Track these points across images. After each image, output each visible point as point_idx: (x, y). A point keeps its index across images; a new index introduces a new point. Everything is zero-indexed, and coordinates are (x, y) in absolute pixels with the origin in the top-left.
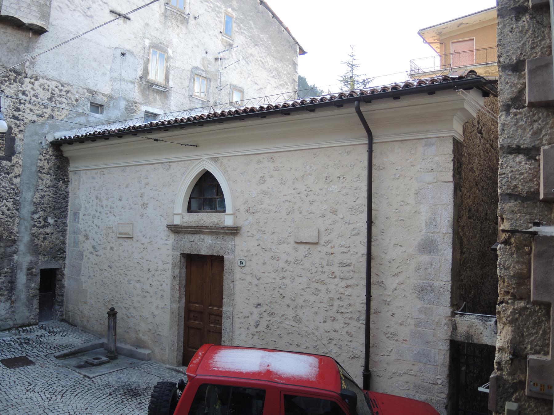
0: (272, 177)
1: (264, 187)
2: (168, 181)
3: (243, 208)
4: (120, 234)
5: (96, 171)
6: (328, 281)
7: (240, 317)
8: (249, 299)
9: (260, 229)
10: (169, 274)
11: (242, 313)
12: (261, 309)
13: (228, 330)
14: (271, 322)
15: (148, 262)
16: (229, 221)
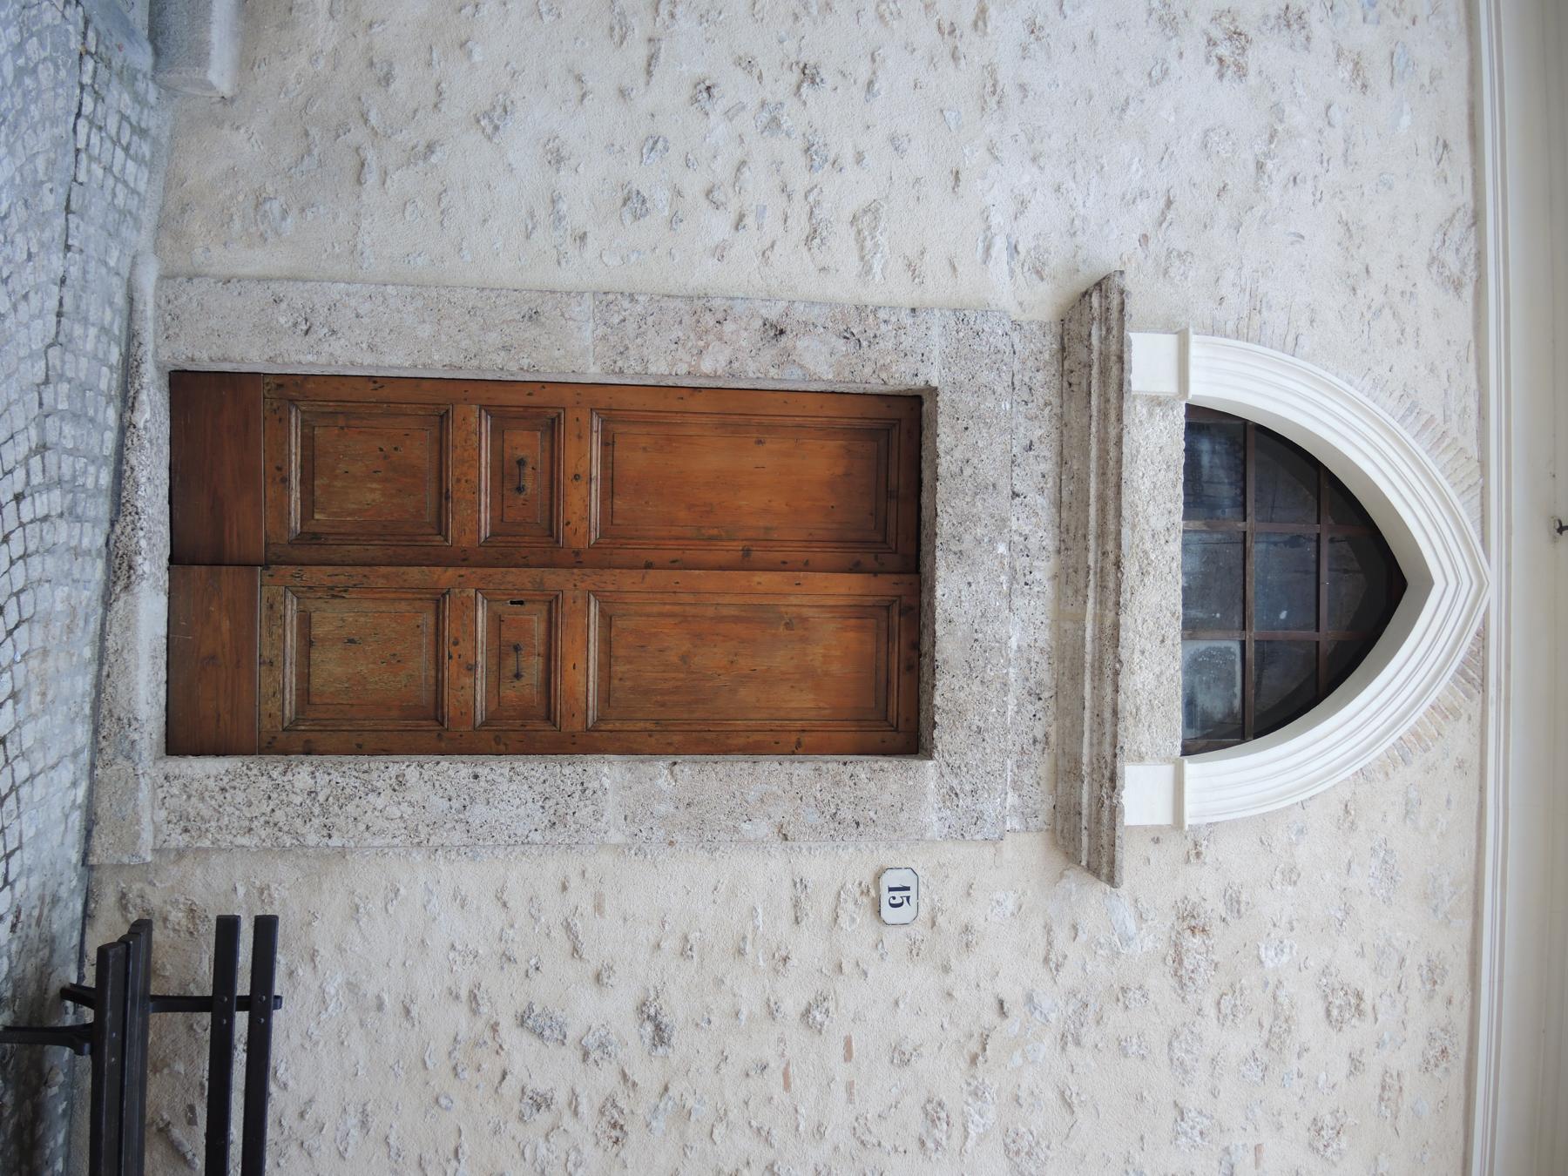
0: (1356, 1065)
1: (1309, 1022)
3: (1204, 885)
8: (685, 952)
9: (1090, 1014)
11: (599, 908)
12: (632, 1036)
13: (479, 812)
14: (567, 1121)
15: (863, 71)
16: (1143, 793)
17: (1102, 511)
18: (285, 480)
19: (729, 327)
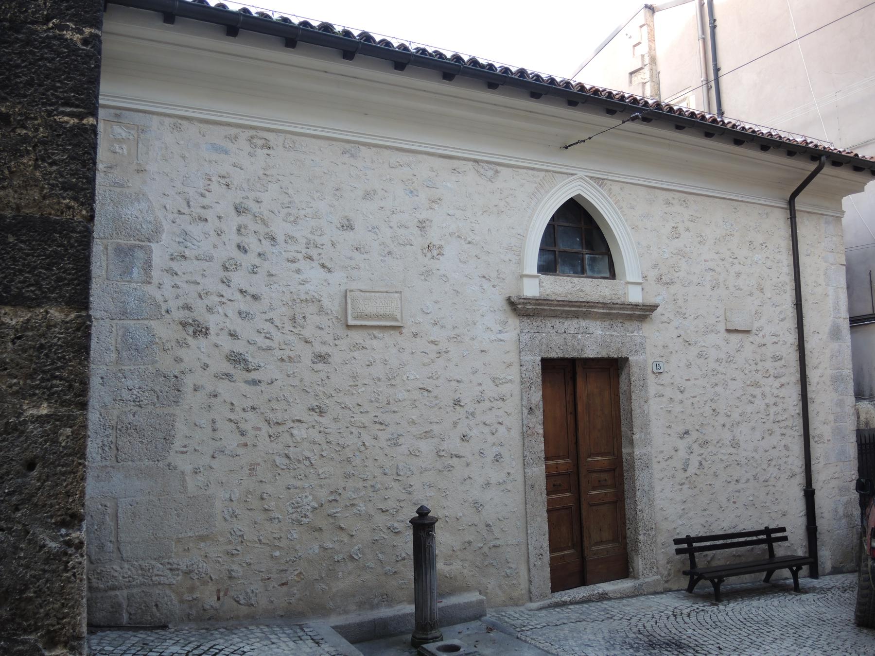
2: (508, 206)
3: (653, 274)
4: (356, 318)
5: (233, 131)
6: (763, 381)
7: (661, 460)
8: (670, 427)
10: (513, 404)
11: (662, 452)
12: (689, 440)
13: (646, 488)
14: (703, 456)
15: (454, 384)
16: (635, 296)
17: (574, 306)
18: (563, 556)
19: (531, 425)
